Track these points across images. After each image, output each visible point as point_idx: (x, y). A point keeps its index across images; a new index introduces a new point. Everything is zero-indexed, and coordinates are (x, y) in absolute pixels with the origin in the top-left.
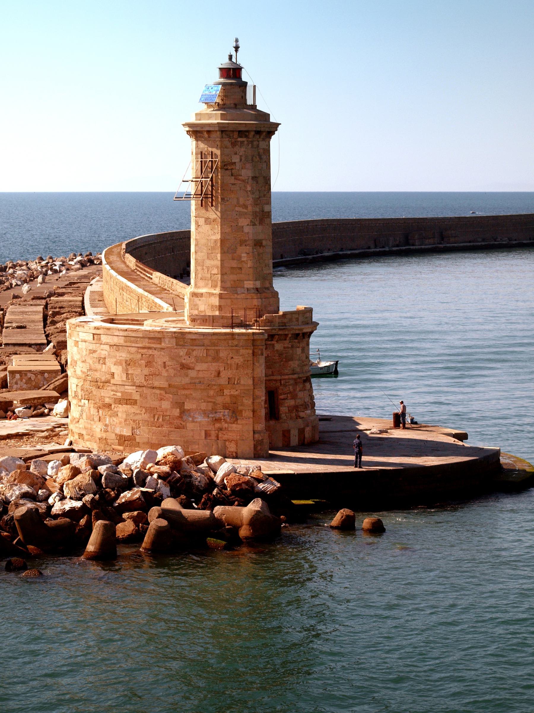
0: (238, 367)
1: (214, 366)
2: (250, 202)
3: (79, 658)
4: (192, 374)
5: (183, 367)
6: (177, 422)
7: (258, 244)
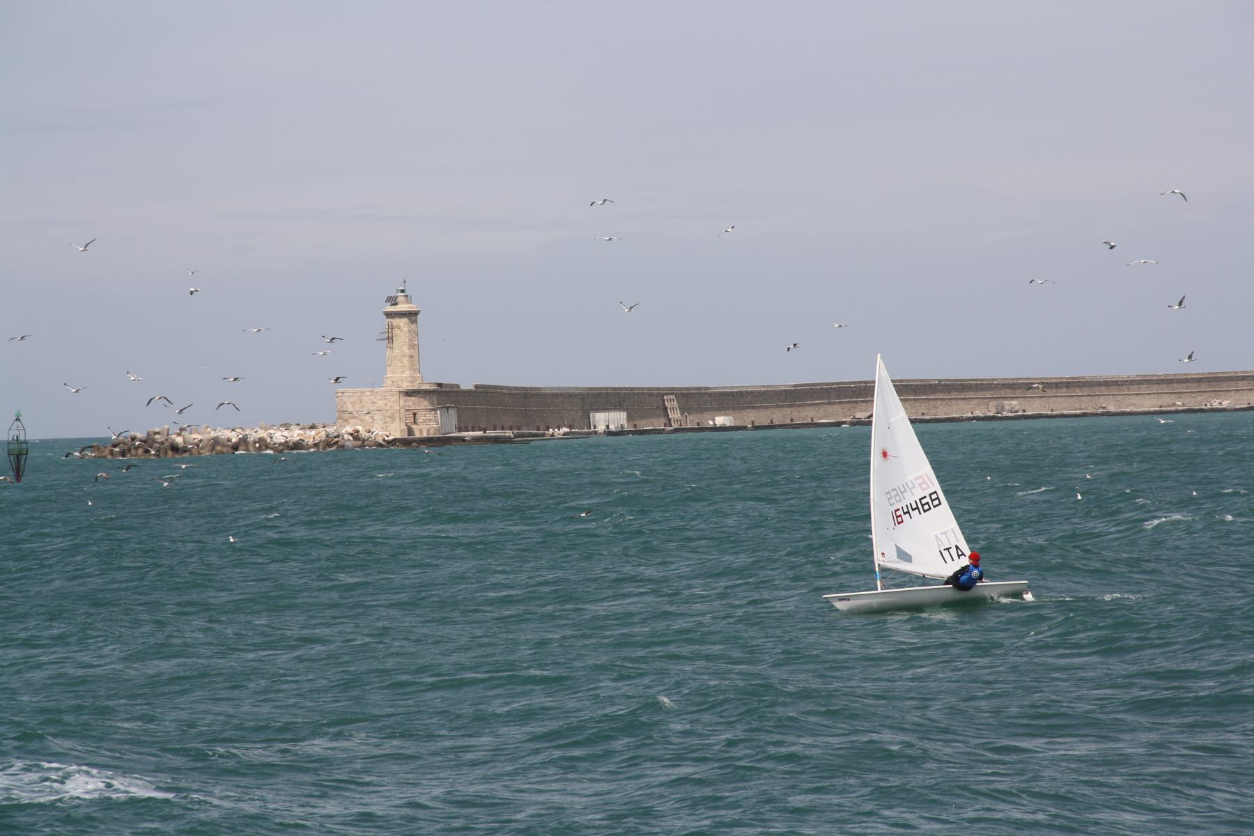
7: (412, 357)
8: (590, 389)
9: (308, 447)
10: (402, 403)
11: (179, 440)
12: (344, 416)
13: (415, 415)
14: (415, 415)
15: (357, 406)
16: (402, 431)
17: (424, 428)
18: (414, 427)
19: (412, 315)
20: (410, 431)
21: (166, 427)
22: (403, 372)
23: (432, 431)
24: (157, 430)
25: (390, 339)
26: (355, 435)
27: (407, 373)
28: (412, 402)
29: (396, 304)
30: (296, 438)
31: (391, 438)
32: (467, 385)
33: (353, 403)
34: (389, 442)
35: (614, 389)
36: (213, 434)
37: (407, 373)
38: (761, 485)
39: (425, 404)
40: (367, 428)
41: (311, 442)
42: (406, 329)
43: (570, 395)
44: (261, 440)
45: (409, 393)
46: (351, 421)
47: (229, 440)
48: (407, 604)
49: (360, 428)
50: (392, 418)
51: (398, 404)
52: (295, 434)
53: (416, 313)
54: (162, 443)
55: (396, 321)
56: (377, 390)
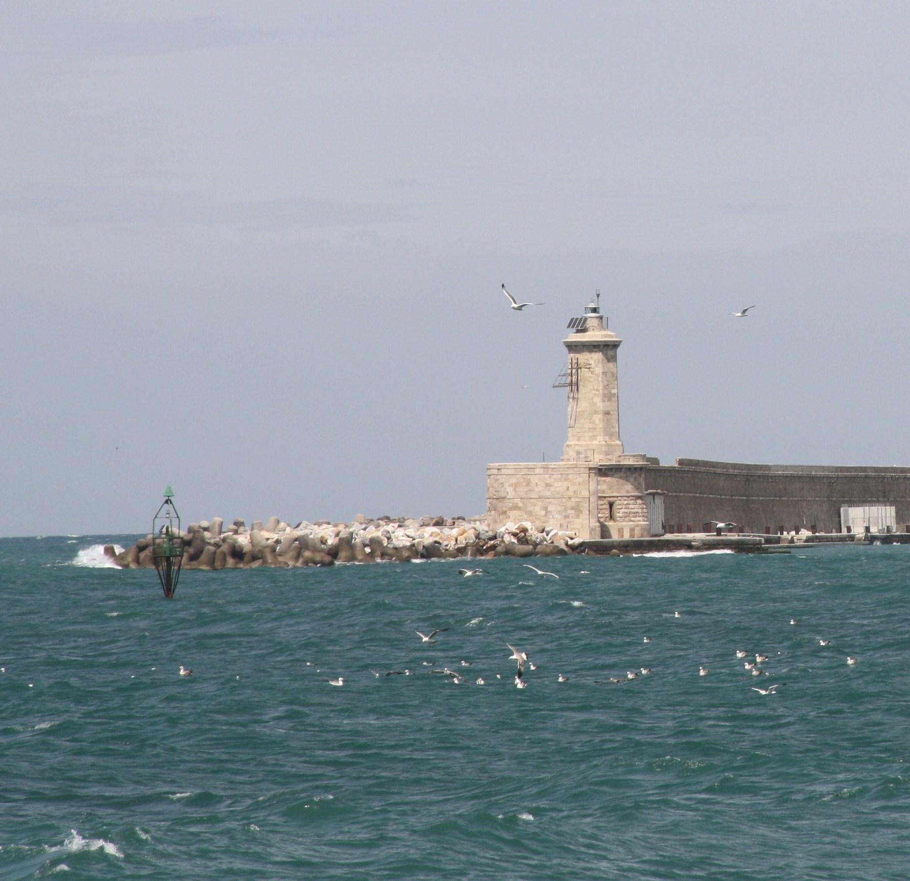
0: (579, 484)
1: (566, 484)
2: (601, 388)
3: (17, 611)
4: (552, 489)
5: (548, 485)
6: (543, 519)
7: (607, 413)
8: (841, 469)
9: (447, 553)
10: (593, 486)
11: (243, 540)
12: (498, 505)
13: (611, 505)
14: (611, 505)
15: (522, 491)
16: (592, 530)
17: (626, 525)
18: (610, 524)
19: (608, 349)
20: (605, 531)
21: (218, 519)
22: (593, 438)
23: (637, 532)
24: (205, 524)
25: (574, 385)
26: (522, 536)
27: (600, 440)
28: (608, 485)
29: (584, 330)
30: (428, 540)
31: (577, 541)
32: (668, 461)
33: (516, 486)
34: (573, 548)
35: (876, 470)
36: (299, 533)
37: (600, 440)
38: (603, 615)
39: (628, 488)
40: (539, 524)
41: (452, 546)
42: (599, 370)
43: (812, 479)
44: (374, 543)
45: (603, 471)
46: (513, 514)
47: (323, 541)
48: (877, 826)
49: (528, 525)
50: (577, 509)
51: (587, 488)
52: (428, 535)
53: (615, 345)
54: (217, 545)
55: (584, 357)
56: (553, 464)
